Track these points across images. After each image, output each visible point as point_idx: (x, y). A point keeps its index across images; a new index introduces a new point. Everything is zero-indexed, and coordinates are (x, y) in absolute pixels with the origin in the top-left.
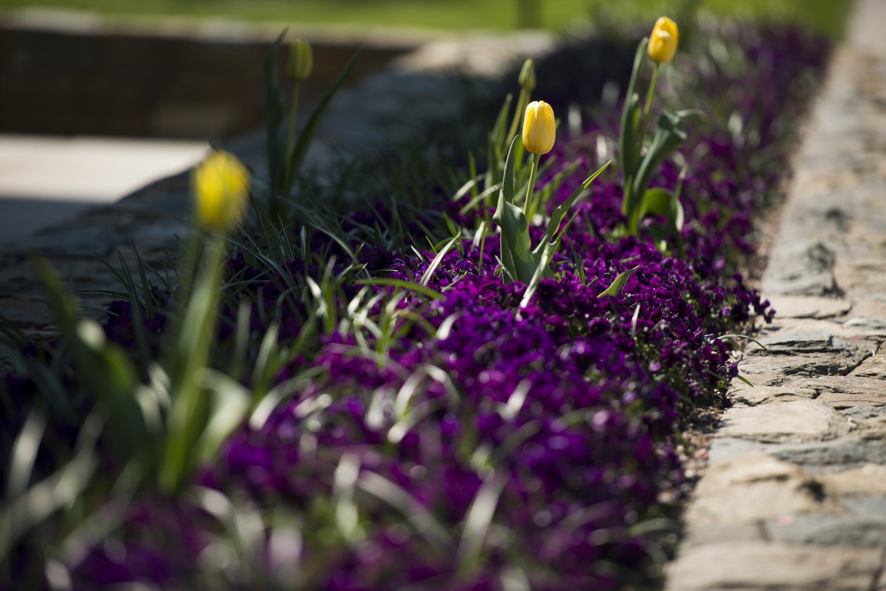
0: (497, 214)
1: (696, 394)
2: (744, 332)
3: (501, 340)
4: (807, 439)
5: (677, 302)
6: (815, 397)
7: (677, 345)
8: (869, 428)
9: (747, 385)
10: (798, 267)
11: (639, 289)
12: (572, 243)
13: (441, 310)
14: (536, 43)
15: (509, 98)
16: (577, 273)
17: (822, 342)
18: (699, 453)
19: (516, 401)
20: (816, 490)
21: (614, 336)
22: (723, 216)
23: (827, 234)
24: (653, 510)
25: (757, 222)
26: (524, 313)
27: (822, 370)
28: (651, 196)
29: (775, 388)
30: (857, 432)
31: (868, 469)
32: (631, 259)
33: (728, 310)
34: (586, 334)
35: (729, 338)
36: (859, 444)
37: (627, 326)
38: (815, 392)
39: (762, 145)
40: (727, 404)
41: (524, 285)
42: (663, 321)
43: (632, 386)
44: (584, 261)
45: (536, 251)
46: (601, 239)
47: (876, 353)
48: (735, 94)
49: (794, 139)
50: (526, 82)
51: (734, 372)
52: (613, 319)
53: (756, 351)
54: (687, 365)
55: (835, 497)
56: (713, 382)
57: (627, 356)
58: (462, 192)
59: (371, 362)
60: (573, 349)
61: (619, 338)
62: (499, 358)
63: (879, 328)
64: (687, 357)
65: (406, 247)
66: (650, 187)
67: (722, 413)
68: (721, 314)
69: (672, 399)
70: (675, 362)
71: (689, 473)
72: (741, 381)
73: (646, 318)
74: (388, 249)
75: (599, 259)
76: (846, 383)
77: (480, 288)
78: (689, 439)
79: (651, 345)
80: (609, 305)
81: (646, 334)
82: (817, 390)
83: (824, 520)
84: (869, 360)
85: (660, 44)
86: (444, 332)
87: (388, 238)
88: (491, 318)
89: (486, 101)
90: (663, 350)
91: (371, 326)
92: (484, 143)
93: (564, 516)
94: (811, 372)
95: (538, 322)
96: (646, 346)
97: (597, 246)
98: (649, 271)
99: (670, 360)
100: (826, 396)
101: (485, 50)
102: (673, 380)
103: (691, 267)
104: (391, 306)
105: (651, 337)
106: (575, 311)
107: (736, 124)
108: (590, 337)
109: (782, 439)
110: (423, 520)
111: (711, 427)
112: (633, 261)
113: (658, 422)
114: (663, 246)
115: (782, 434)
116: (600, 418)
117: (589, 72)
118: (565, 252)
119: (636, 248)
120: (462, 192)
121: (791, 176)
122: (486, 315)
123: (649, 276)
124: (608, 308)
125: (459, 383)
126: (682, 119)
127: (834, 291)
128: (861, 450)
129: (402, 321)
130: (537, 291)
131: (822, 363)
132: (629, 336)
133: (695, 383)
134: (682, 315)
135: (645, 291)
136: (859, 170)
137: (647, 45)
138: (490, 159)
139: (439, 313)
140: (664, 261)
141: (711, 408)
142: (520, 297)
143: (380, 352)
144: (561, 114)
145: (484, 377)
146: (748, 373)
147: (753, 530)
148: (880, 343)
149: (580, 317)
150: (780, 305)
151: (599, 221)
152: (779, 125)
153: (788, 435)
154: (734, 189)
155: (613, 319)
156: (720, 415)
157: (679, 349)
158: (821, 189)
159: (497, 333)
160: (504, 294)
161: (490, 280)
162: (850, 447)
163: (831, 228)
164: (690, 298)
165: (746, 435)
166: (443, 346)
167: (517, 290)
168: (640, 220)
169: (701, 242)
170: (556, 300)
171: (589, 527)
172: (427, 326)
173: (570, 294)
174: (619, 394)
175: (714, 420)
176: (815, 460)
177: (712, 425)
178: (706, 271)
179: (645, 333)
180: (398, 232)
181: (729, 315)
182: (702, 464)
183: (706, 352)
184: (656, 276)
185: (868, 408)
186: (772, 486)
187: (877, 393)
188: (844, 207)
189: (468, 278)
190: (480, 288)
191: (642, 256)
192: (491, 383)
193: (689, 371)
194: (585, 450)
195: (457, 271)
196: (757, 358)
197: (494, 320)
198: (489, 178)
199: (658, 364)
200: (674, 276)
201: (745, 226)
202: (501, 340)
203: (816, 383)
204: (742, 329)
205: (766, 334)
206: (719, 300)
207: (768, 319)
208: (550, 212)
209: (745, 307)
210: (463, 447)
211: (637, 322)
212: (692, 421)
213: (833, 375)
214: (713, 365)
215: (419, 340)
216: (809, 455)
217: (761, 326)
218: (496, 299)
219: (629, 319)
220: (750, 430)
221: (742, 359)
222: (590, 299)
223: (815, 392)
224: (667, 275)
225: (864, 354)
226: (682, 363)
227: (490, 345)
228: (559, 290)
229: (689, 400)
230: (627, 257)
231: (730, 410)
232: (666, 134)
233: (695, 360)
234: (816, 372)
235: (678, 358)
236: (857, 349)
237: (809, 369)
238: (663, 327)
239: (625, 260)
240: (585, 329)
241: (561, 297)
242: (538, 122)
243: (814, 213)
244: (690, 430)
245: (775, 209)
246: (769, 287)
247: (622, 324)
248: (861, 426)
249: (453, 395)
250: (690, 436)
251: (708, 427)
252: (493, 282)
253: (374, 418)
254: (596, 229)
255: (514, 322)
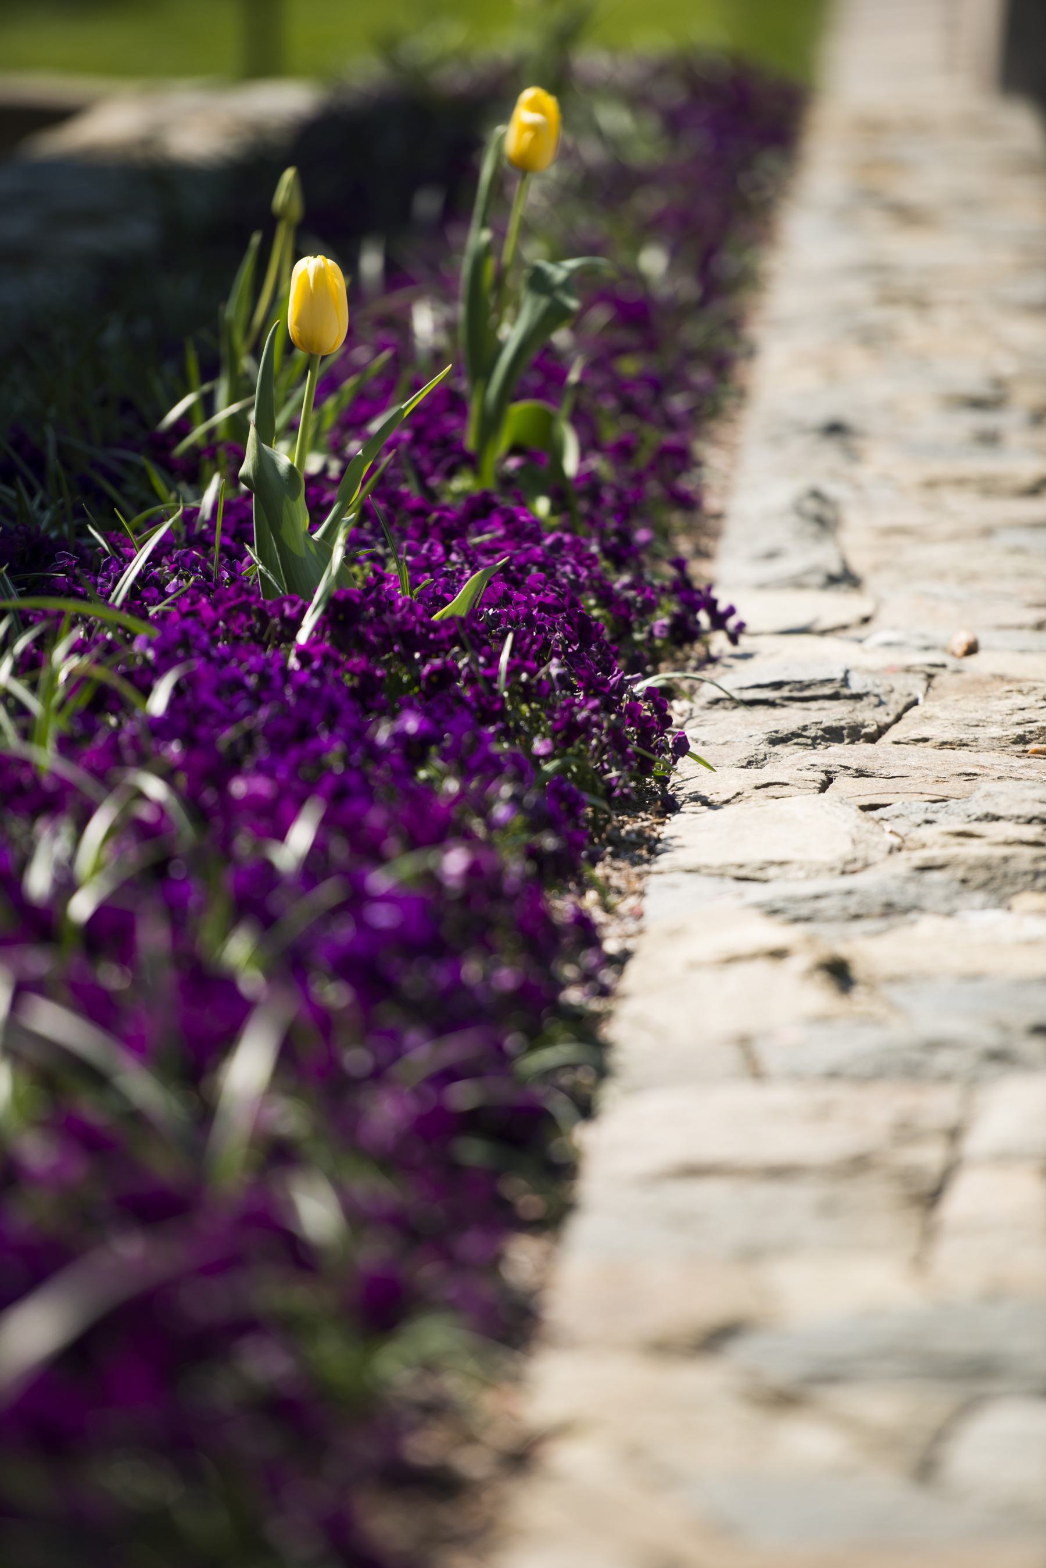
0: (247, 468)
1: (617, 792)
2: (692, 663)
3: (263, 714)
4: (815, 871)
5: (576, 620)
6: (824, 787)
7: (581, 707)
8: (924, 846)
9: (704, 768)
10: (780, 534)
11: (507, 600)
12: (380, 508)
13: (150, 654)
14: (284, 101)
15: (256, 239)
16: (392, 566)
17: (831, 681)
18: (625, 905)
19: (302, 835)
20: (839, 973)
21: (467, 693)
22: (642, 441)
23: (822, 466)
24: (554, 1027)
25: (703, 450)
26: (303, 655)
27: (833, 735)
28: (519, 412)
29: (752, 771)
30: (904, 854)
31: (926, 926)
32: (487, 537)
33: (663, 626)
34: (416, 689)
35: (668, 679)
36: (908, 880)
37: (490, 672)
38: (823, 777)
39: (704, 302)
40: (670, 806)
41: (301, 602)
42: (555, 661)
43: (506, 790)
44: (405, 544)
45: (317, 535)
46: (431, 495)
47: (926, 695)
48: (650, 202)
49: (748, 280)
50: (286, 207)
51: (682, 747)
52: (465, 660)
53: (716, 701)
54: (600, 741)
55: (872, 985)
56: (646, 767)
57: (492, 729)
58: (174, 414)
59: (26, 764)
60: (397, 726)
61: (477, 695)
62: (262, 751)
63: (927, 648)
64: (600, 727)
65: (77, 521)
66: (516, 399)
67: (663, 824)
68: (651, 634)
69: (575, 805)
70: (577, 736)
71: (611, 946)
72: (693, 761)
73: (525, 657)
74: (43, 526)
75: (431, 540)
76: (877, 757)
77: (219, 613)
78: (607, 878)
79: (533, 705)
80: (457, 634)
81: (526, 685)
82: (827, 772)
83: (855, 1032)
84: (913, 712)
85: (528, 136)
86: (158, 702)
87: (43, 507)
88: (245, 667)
89: (208, 224)
90: (557, 716)
91: (19, 689)
92: (208, 317)
93: (397, 1055)
94: (815, 739)
95: (329, 672)
96: (524, 708)
97: (426, 513)
98: (522, 559)
99: (568, 732)
100: (843, 783)
101: (197, 120)
102: (574, 769)
103: (594, 549)
104: (59, 652)
105: (534, 690)
106: (396, 648)
107: (653, 261)
108: (425, 695)
109: (772, 872)
110: (141, 1086)
111: (644, 852)
112: (492, 541)
113: (555, 855)
114: (542, 506)
115: (772, 863)
116: (455, 862)
117: (390, 167)
118: (367, 525)
119: (496, 517)
120: (174, 414)
121: (751, 353)
122: (234, 663)
123: (523, 569)
124: (455, 640)
125: (191, 800)
126: (573, 272)
127: (844, 579)
128: (912, 889)
129: (77, 681)
130: (325, 612)
131: (836, 724)
132: (494, 692)
133: (614, 773)
134: (585, 645)
135: (518, 603)
136: (871, 339)
137: (502, 138)
138: (224, 350)
139: (145, 660)
140: (548, 541)
141: (642, 814)
142: (295, 624)
143: (42, 743)
144: (349, 265)
145: (239, 787)
146: (704, 744)
147: (732, 1056)
148: (930, 677)
149: (406, 659)
150: (753, 609)
151: (426, 465)
152: (728, 262)
153: (782, 864)
154: (658, 385)
155: (465, 660)
156: (659, 829)
157: (584, 714)
158: (807, 379)
159: (257, 699)
160: (264, 619)
161: (239, 595)
162: (893, 885)
163: (830, 454)
164: (595, 606)
165: (706, 867)
166: (161, 729)
167: (288, 611)
168: (501, 459)
169: (609, 495)
170: (362, 629)
171: (448, 1075)
172: (128, 691)
173: (387, 617)
174: (483, 810)
175: (649, 839)
176: (832, 912)
177: (644, 849)
178: (622, 554)
179: (522, 684)
180: (60, 494)
181: (665, 634)
182: (631, 926)
183: (633, 709)
184: (534, 570)
185: (918, 809)
186: (762, 968)
187: (932, 775)
188: (849, 415)
189: (198, 587)
190: (221, 610)
191: (508, 532)
192: (252, 800)
193: (603, 751)
194: (435, 927)
195: (175, 571)
196: (719, 714)
197: (249, 672)
198: (223, 389)
199: (548, 741)
200: (568, 568)
201: (681, 458)
202: (263, 714)
203: (827, 761)
204: (688, 658)
205: (729, 666)
206: (650, 607)
207: (734, 639)
208: (337, 449)
209: (691, 618)
210: (207, 930)
211: (509, 664)
212: (610, 842)
213: (852, 742)
214: (644, 739)
215: (114, 713)
216: (822, 904)
217: (721, 651)
218: (250, 628)
219: (493, 659)
220: (715, 858)
221: (691, 718)
222: (422, 625)
223: (823, 777)
224: (554, 566)
225: (905, 701)
226: (590, 737)
227: (246, 723)
228: (367, 610)
229: (605, 806)
230: (480, 533)
231: (676, 818)
232: (544, 302)
233: (614, 731)
234: (823, 738)
235: (582, 730)
236: (892, 691)
237: (811, 733)
238: (554, 671)
239: (477, 540)
240: (416, 680)
241: (370, 622)
242: (316, 297)
243: (801, 428)
244: (608, 859)
245: (731, 421)
246: (731, 575)
247: (481, 670)
248: (908, 844)
249: (185, 831)
250: (608, 871)
251: (638, 852)
252: (244, 597)
253: (39, 881)
254: (422, 478)
255: (286, 674)
